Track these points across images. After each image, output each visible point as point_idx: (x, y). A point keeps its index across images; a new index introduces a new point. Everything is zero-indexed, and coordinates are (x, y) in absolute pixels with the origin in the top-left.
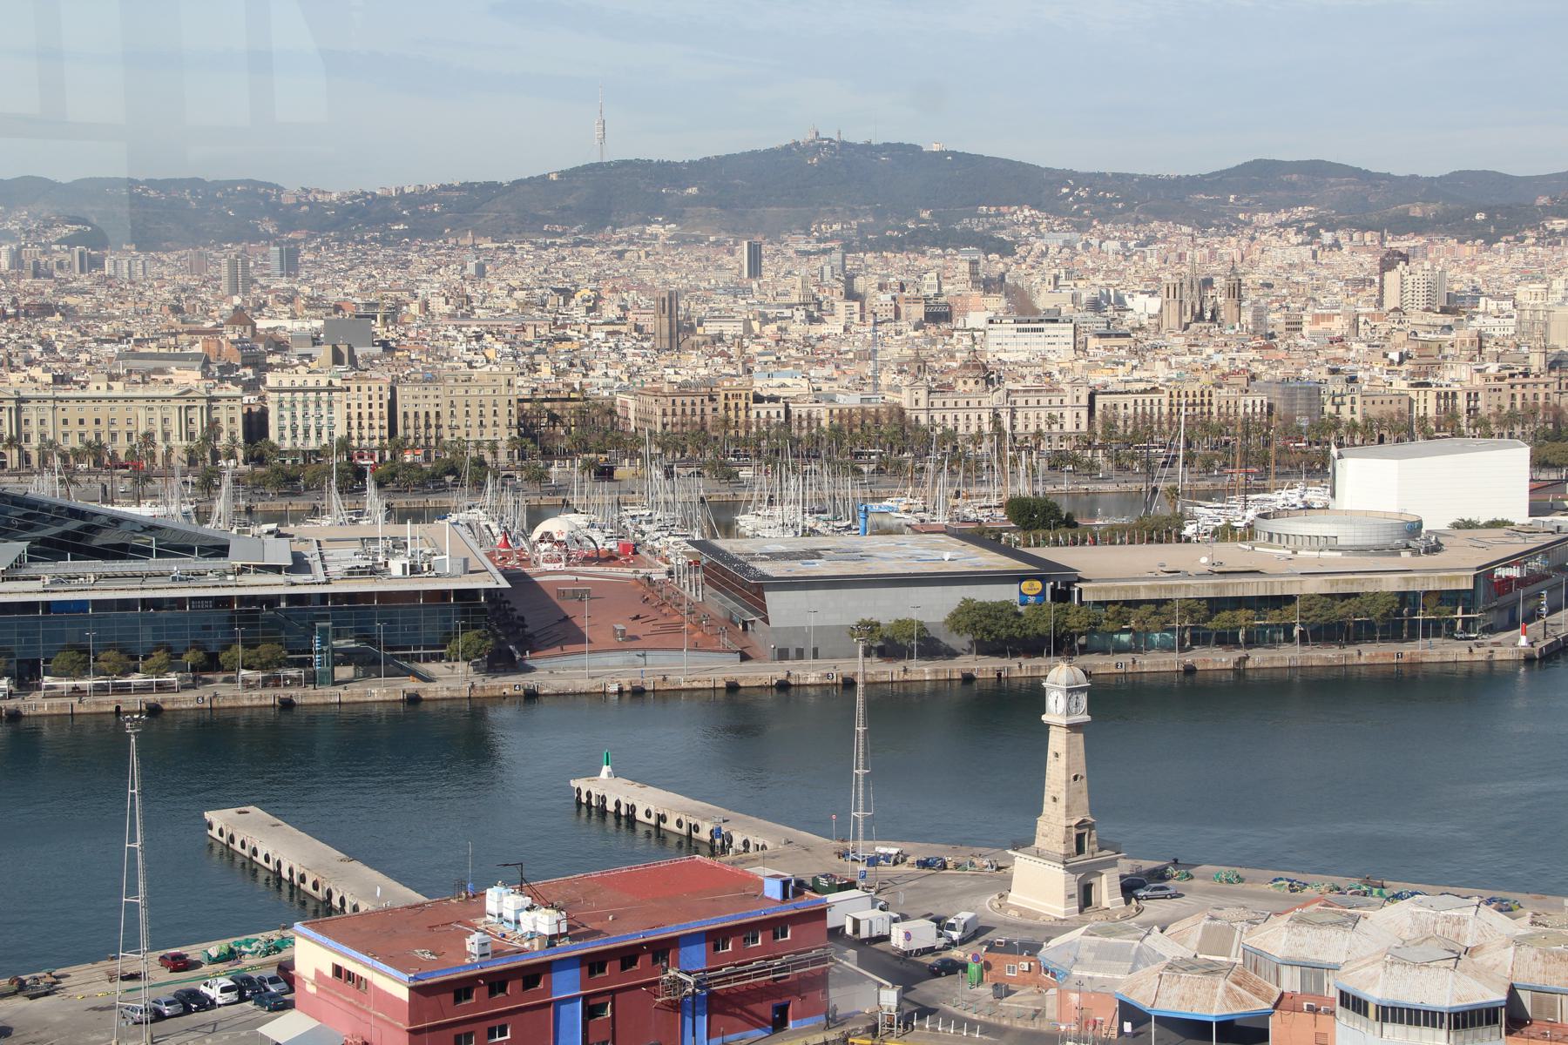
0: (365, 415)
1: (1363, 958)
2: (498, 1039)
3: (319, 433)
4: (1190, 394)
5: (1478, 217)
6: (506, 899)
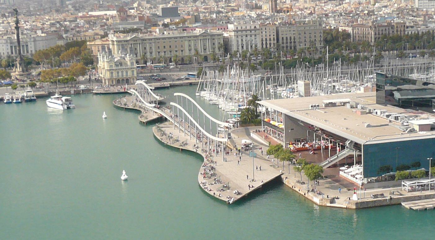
0: (268, 39)
3: (242, 47)
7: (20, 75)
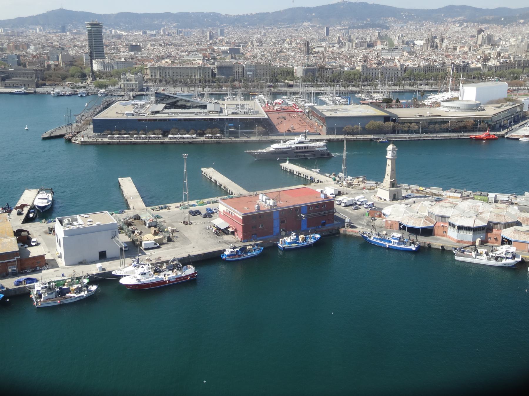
1: (456, 215)
2: (261, 227)
4: (429, 67)
5: (502, 19)
6: (264, 197)
7: (90, 82)
